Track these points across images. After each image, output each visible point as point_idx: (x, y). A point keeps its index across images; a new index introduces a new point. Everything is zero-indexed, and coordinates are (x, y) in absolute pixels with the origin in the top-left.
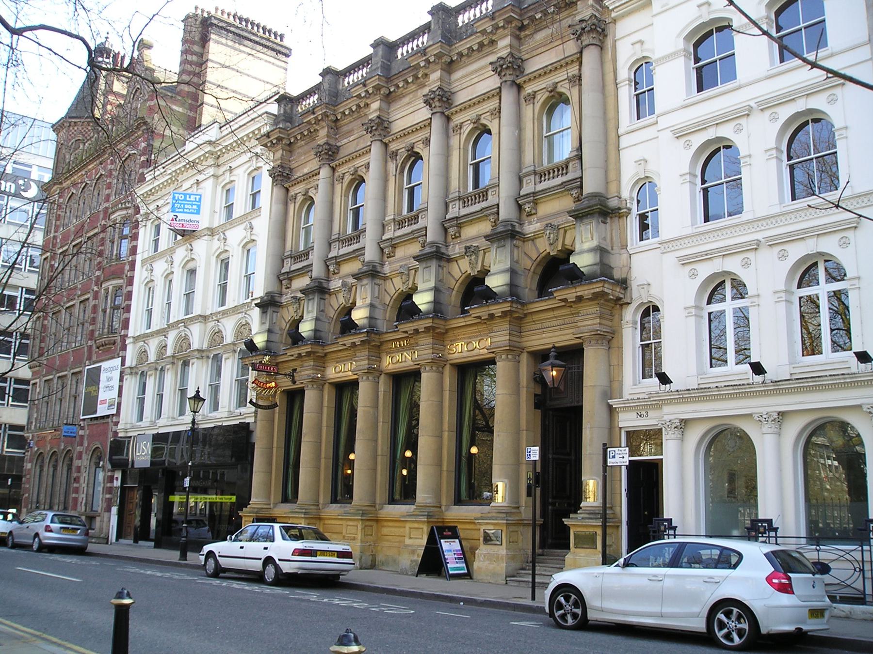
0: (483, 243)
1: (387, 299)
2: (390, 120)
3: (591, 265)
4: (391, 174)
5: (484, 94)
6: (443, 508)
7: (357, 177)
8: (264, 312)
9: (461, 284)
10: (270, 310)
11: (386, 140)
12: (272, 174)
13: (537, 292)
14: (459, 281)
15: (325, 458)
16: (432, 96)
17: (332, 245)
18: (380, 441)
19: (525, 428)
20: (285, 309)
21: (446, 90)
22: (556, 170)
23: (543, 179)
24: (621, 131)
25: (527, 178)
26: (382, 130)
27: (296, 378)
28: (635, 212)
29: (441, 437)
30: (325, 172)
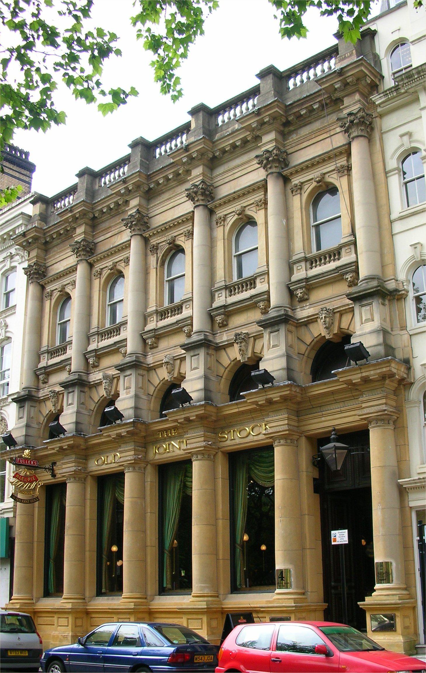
0: (255, 329)
1: (152, 390)
2: (150, 215)
3: (375, 346)
4: (152, 267)
5: (249, 186)
6: (221, 596)
7: (116, 272)
8: (21, 407)
9: (229, 371)
10: (27, 405)
11: (146, 235)
12: (27, 271)
13: (311, 376)
14: (228, 369)
15: (89, 551)
16: (195, 189)
17: (91, 338)
18: (148, 532)
19: (306, 512)
20: (43, 404)
21: (209, 184)
22: (327, 256)
23: (314, 265)
24: (394, 216)
25: (298, 265)
26: (142, 225)
27: (56, 472)
28: (411, 295)
29: (215, 525)
30: (81, 269)
